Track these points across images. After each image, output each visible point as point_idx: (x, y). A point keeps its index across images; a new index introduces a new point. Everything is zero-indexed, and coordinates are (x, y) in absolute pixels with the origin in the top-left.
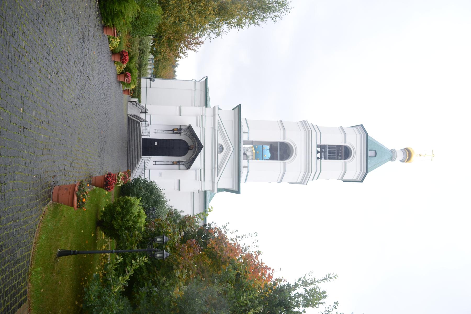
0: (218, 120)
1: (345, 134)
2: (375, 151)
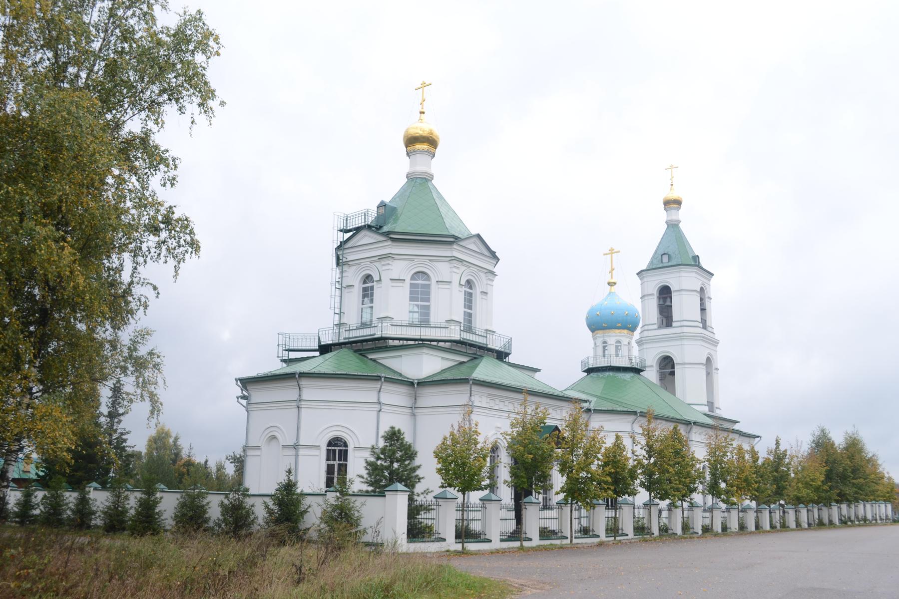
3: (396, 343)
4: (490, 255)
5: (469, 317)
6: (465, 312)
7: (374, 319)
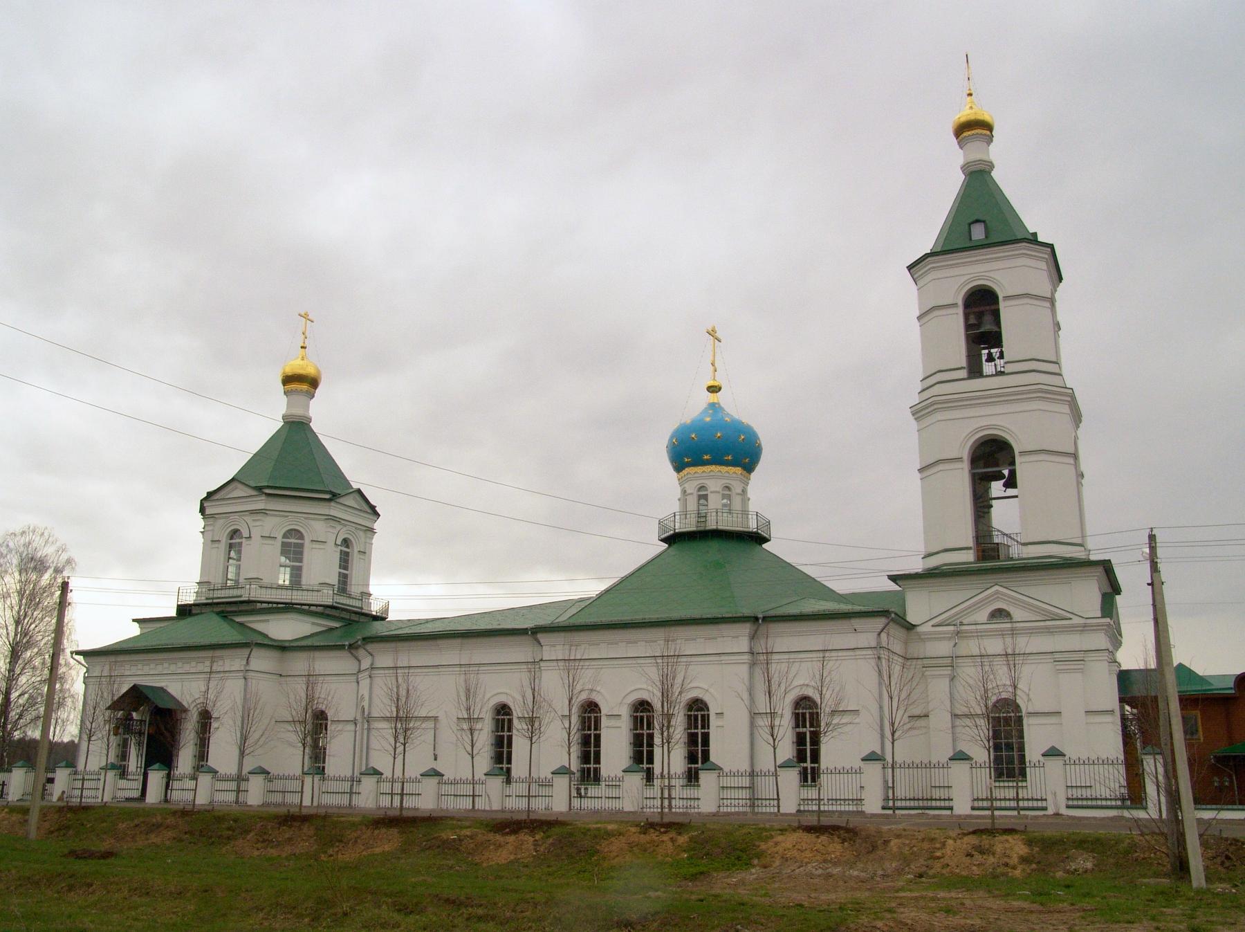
0: (933, 626)
1: (934, 310)
2: (970, 225)
3: (265, 605)
4: (369, 511)
5: (344, 580)
6: (340, 573)
7: (241, 580)
